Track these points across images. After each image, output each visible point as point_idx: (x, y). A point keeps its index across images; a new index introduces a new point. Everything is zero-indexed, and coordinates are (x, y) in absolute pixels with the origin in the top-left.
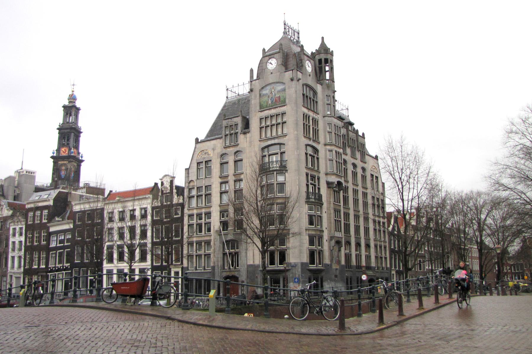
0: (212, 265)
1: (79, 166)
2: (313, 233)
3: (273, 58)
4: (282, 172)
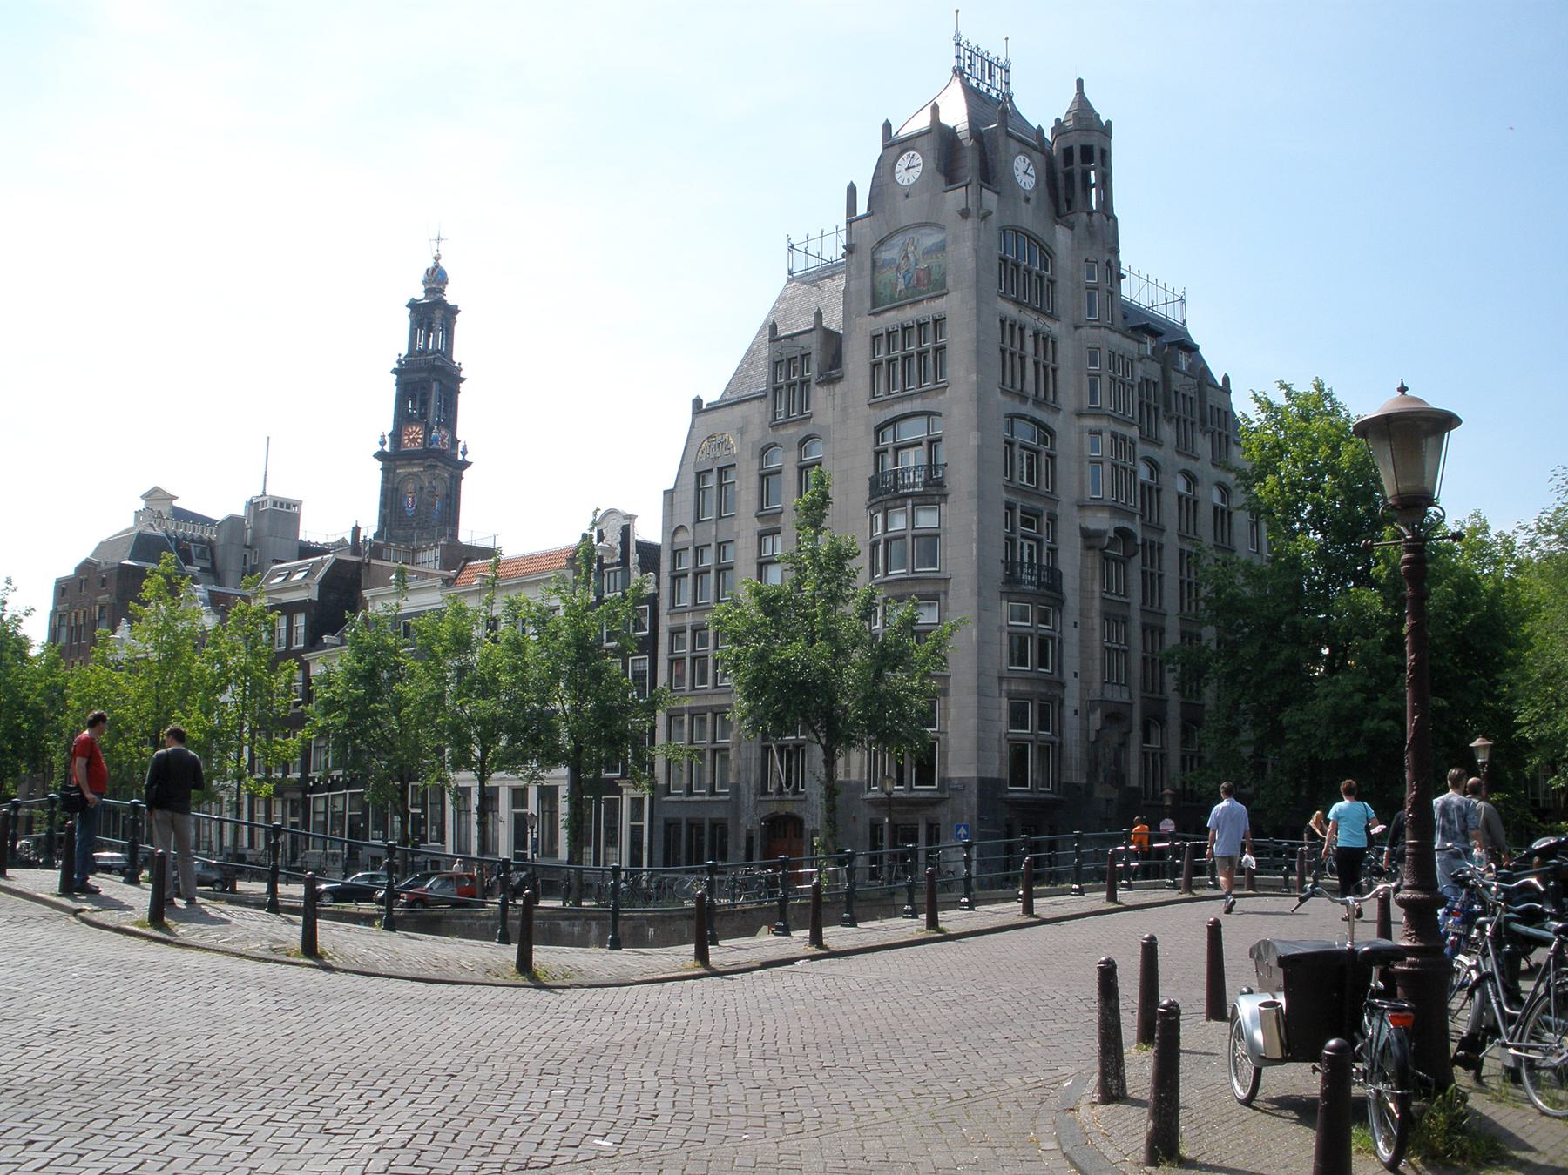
0: (732, 780)
1: (456, 481)
2: (1024, 688)
3: (913, 149)
4: (930, 500)
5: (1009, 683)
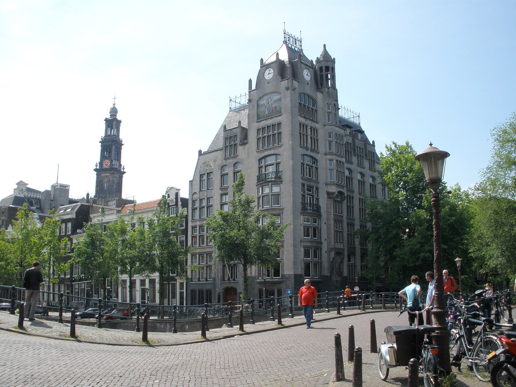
0: (213, 276)
1: (121, 178)
2: (308, 244)
3: (270, 67)
5: (303, 243)
